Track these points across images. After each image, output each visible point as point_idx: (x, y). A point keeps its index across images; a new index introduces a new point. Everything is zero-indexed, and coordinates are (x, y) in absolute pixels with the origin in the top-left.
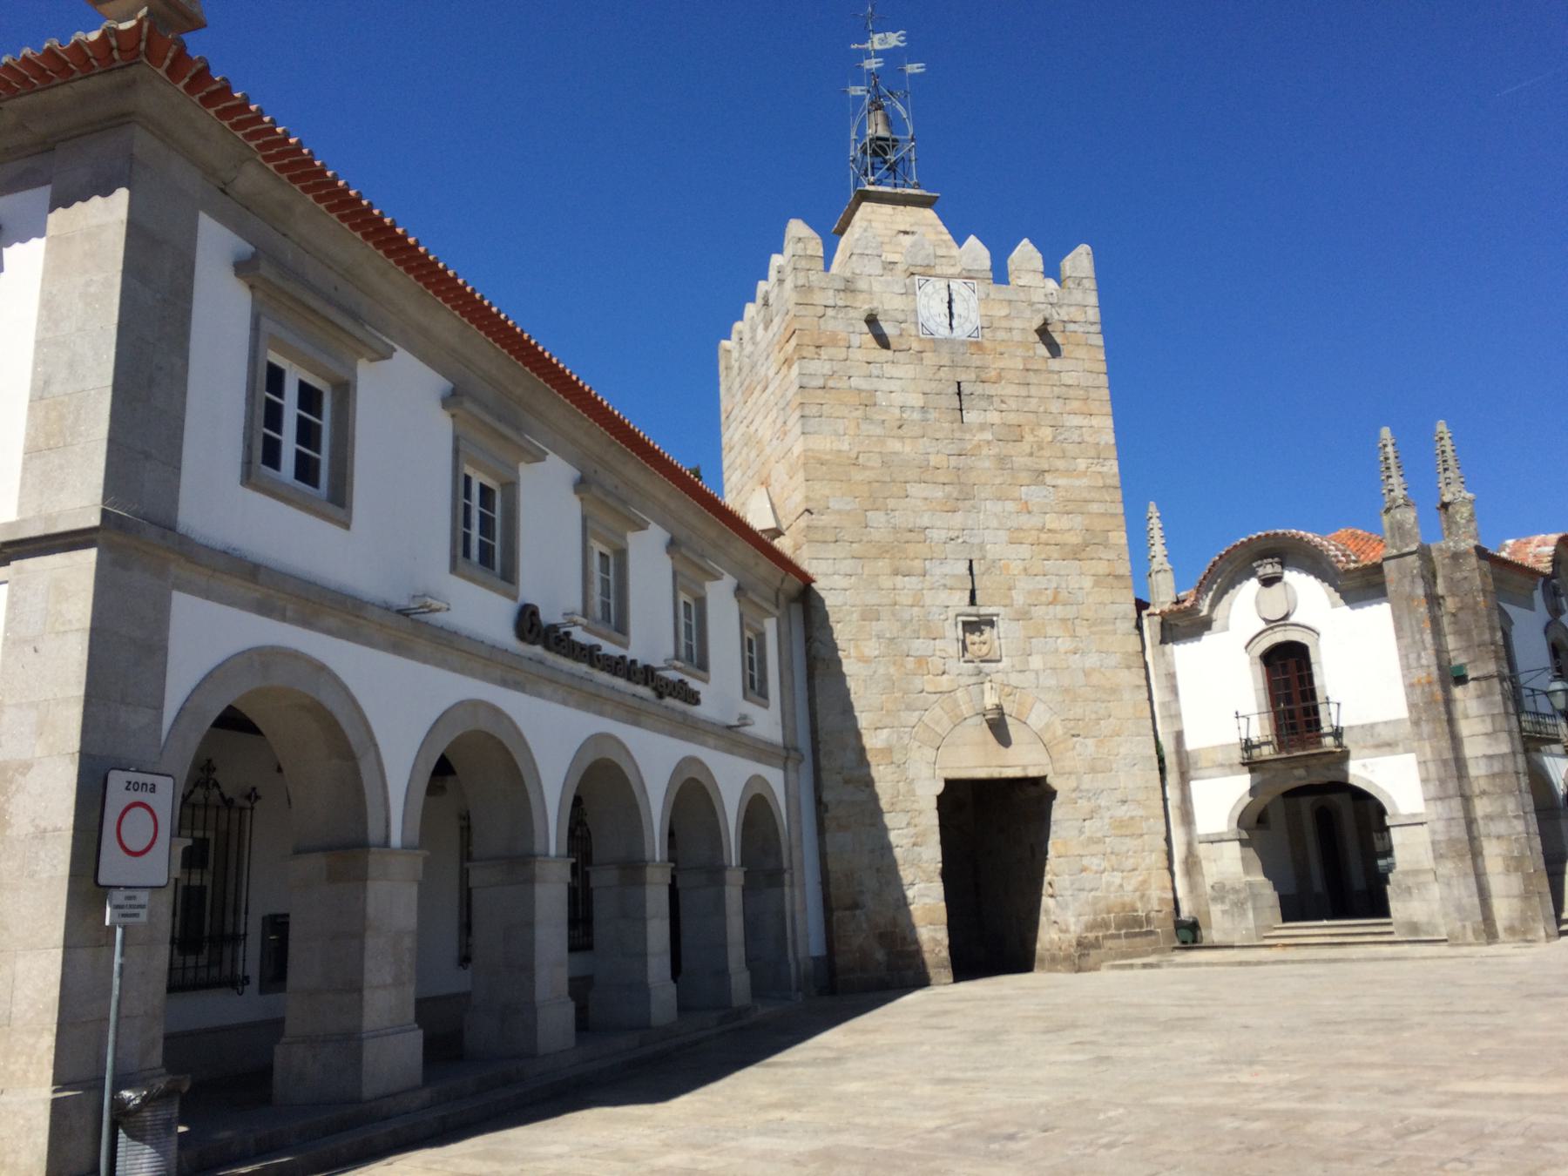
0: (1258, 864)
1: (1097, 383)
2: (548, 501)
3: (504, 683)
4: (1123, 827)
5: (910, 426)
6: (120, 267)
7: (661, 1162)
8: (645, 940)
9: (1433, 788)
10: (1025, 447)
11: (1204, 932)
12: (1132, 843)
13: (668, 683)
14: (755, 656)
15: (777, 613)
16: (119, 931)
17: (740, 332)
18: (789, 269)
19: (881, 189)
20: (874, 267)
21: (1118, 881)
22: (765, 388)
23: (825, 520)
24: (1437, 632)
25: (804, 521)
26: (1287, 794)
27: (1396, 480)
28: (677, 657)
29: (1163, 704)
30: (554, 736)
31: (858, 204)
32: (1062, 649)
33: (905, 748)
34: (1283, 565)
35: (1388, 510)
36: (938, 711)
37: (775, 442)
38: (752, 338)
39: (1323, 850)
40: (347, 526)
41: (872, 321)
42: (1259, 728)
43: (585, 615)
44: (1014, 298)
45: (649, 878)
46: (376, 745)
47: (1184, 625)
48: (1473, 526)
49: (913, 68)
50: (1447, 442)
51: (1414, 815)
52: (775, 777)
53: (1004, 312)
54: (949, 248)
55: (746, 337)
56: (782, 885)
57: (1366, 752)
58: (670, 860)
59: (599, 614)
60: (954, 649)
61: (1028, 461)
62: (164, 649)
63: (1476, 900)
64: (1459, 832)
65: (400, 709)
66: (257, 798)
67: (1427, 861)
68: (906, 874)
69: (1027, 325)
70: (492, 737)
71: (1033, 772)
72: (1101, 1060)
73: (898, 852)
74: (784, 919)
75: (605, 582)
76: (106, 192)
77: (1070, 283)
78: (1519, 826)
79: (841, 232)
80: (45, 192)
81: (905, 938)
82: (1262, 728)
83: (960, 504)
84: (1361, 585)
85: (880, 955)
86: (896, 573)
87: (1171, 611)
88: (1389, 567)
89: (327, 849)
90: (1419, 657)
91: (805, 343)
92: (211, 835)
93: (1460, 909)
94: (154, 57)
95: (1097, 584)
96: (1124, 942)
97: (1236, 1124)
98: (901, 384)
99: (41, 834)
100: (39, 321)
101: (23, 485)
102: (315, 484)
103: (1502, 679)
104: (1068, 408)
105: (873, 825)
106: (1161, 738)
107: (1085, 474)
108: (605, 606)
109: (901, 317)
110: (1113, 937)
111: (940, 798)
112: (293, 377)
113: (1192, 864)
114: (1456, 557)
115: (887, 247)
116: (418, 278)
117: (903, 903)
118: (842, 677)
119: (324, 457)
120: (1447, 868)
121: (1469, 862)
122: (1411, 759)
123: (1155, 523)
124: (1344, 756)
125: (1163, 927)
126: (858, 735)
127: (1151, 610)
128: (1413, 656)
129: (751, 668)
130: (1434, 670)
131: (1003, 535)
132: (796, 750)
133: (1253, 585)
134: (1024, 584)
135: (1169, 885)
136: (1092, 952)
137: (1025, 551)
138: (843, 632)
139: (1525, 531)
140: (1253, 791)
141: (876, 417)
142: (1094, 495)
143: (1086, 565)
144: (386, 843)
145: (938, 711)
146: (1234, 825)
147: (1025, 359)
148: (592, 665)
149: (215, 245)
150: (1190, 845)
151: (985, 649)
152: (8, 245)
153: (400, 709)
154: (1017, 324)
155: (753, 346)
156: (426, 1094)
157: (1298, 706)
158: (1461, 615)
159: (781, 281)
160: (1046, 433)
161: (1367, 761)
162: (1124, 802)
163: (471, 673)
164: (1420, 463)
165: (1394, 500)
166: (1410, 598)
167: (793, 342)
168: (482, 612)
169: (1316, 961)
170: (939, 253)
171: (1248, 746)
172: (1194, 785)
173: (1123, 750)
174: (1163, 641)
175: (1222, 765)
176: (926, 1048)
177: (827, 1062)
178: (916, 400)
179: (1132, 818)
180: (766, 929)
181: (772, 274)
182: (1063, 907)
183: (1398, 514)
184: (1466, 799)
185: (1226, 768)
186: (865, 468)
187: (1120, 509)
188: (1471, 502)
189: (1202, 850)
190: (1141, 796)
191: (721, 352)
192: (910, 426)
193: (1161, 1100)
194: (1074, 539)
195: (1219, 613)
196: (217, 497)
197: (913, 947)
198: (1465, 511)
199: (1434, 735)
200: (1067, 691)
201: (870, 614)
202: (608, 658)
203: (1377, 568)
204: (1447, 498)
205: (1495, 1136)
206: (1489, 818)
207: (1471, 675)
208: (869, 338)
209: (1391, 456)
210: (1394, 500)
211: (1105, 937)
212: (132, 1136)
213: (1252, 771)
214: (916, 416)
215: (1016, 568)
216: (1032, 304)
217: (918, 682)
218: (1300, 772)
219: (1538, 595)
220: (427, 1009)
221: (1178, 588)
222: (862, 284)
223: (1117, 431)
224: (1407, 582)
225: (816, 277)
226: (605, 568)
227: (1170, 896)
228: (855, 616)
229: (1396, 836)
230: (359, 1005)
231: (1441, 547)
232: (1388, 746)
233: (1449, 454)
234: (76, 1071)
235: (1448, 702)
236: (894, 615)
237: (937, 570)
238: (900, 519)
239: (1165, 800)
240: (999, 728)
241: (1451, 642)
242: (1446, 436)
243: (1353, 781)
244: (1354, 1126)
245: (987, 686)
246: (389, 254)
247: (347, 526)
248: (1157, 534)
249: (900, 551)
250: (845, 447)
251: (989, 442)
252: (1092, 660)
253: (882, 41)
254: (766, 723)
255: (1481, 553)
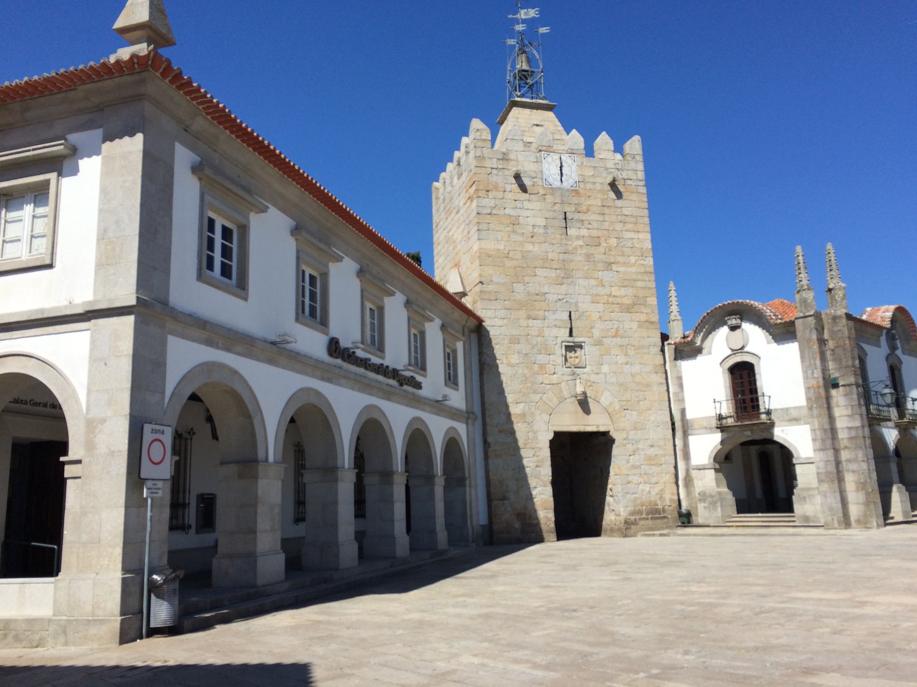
0: (724, 482)
1: (642, 214)
2: (344, 282)
3: (322, 379)
4: (652, 460)
5: (539, 236)
6: (140, 174)
7: (407, 617)
8: (393, 513)
9: (818, 444)
10: (601, 249)
11: (694, 518)
12: (655, 469)
13: (405, 378)
14: (451, 362)
15: (463, 339)
16: (149, 500)
17: (444, 179)
18: (472, 146)
19: (524, 100)
20: (519, 146)
21: (648, 489)
22: (458, 212)
23: (490, 288)
24: (823, 359)
25: (478, 288)
26: (744, 444)
27: (803, 275)
28: (410, 364)
29: (675, 393)
30: (347, 405)
31: (511, 108)
32: (620, 362)
33: (532, 413)
34: (742, 319)
35: (798, 292)
36: (550, 394)
37: (463, 243)
38: (451, 183)
39: (760, 476)
40: (246, 299)
41: (517, 177)
42: (727, 408)
43: (362, 343)
44: (597, 165)
45: (395, 481)
46: (261, 412)
47: (687, 350)
48: (844, 302)
49: (543, 30)
50: (832, 255)
51: (809, 458)
52: (461, 428)
53: (591, 173)
54: (561, 134)
55: (448, 182)
56: (465, 486)
57: (784, 423)
58: (406, 471)
59: (369, 342)
60: (561, 360)
61: (603, 257)
62: (165, 364)
63: (840, 505)
64: (832, 468)
65: (272, 392)
66: (194, 433)
67: (814, 483)
68: (532, 482)
69: (603, 181)
70: (315, 406)
71: (602, 429)
72: (625, 579)
73: (528, 470)
74: (465, 504)
75: (372, 324)
76: (132, 135)
77: (628, 158)
78: (864, 466)
79: (501, 123)
80: (98, 133)
81: (530, 517)
82: (728, 408)
83: (565, 281)
84: (783, 332)
85: (517, 525)
86: (529, 318)
87: (680, 343)
88: (798, 323)
89: (237, 462)
90: (813, 373)
91: (480, 188)
93: (831, 509)
94: (155, 67)
95: (640, 326)
96: (650, 522)
97: (682, 607)
98: (533, 213)
99: (112, 453)
100: (100, 199)
101: (95, 282)
102: (230, 278)
103: (858, 386)
104: (626, 228)
105: (515, 455)
106: (673, 412)
107: (634, 265)
108: (373, 337)
109: (534, 175)
110: (644, 519)
111: (551, 442)
112: (219, 223)
113: (688, 481)
114: (835, 318)
115: (526, 134)
116: (279, 169)
117: (530, 498)
118: (499, 374)
119: (234, 264)
120: (825, 487)
121: (836, 485)
122: (807, 428)
123: (673, 293)
124: (772, 425)
125: (672, 514)
126: (507, 406)
127: (670, 341)
128: (809, 372)
129: (449, 369)
130: (821, 380)
131: (588, 298)
132: (473, 413)
133: (725, 330)
134: (599, 325)
135: (676, 492)
136: (633, 527)
137: (600, 307)
138: (499, 350)
139: (877, 303)
140: (722, 442)
141: (519, 231)
142: (639, 277)
143: (634, 316)
144: (266, 460)
145: (550, 394)
146: (712, 460)
147: (603, 200)
148: (366, 369)
149: (183, 157)
151: (577, 361)
152: (82, 158)
153: (272, 392)
154: (598, 180)
155: (451, 187)
156: (286, 585)
157: (748, 397)
158: (836, 351)
159: (467, 153)
160: (613, 242)
161: (784, 428)
162: (652, 446)
163: (307, 374)
164: (816, 265)
165: (802, 286)
166: (809, 340)
167: (474, 188)
168: (312, 342)
169: (753, 535)
170: (557, 137)
171: (720, 418)
172: (690, 438)
173: (652, 418)
174: (676, 359)
175: (706, 428)
176: (539, 572)
177: (487, 577)
178: (542, 222)
179: (656, 455)
180: (456, 510)
181: (463, 148)
182: (618, 502)
183: (804, 294)
184: (836, 451)
185: (708, 430)
186: (512, 259)
187: (653, 285)
188: (844, 288)
189: (694, 473)
190: (661, 443)
191: (433, 189)
192: (539, 236)
193: (650, 597)
194: (627, 301)
195: (706, 344)
196: (189, 291)
197: (535, 522)
198: (841, 293)
199: (820, 415)
200: (622, 385)
201: (514, 340)
202: (374, 365)
203: (792, 323)
204: (831, 286)
205: (800, 615)
206: (849, 461)
207: (841, 383)
208: (515, 187)
209: (801, 261)
210: (802, 286)
211: (640, 519)
212: (158, 597)
213: (722, 431)
214: (541, 231)
215: (595, 316)
216: (606, 169)
217: (540, 378)
218: (748, 433)
219: (883, 339)
220: (286, 544)
221: (685, 329)
222: (512, 156)
223: (653, 241)
224: (807, 331)
225: (487, 152)
226: (372, 317)
227: (676, 498)
228: (506, 341)
229: (799, 469)
230: (254, 542)
231: (827, 312)
232: (795, 420)
233: (833, 262)
234: (132, 566)
235: (828, 398)
236: (527, 341)
237: (551, 317)
238: (532, 288)
239: (675, 446)
240: (584, 404)
241: (831, 365)
242: (832, 252)
243: (776, 439)
244: (737, 610)
245: (578, 381)
246: (265, 158)
247: (246, 299)
248: (674, 299)
249: (531, 306)
250: (502, 247)
251: (581, 246)
252: (636, 368)
253: (526, 14)
254: (457, 399)
255: (849, 317)
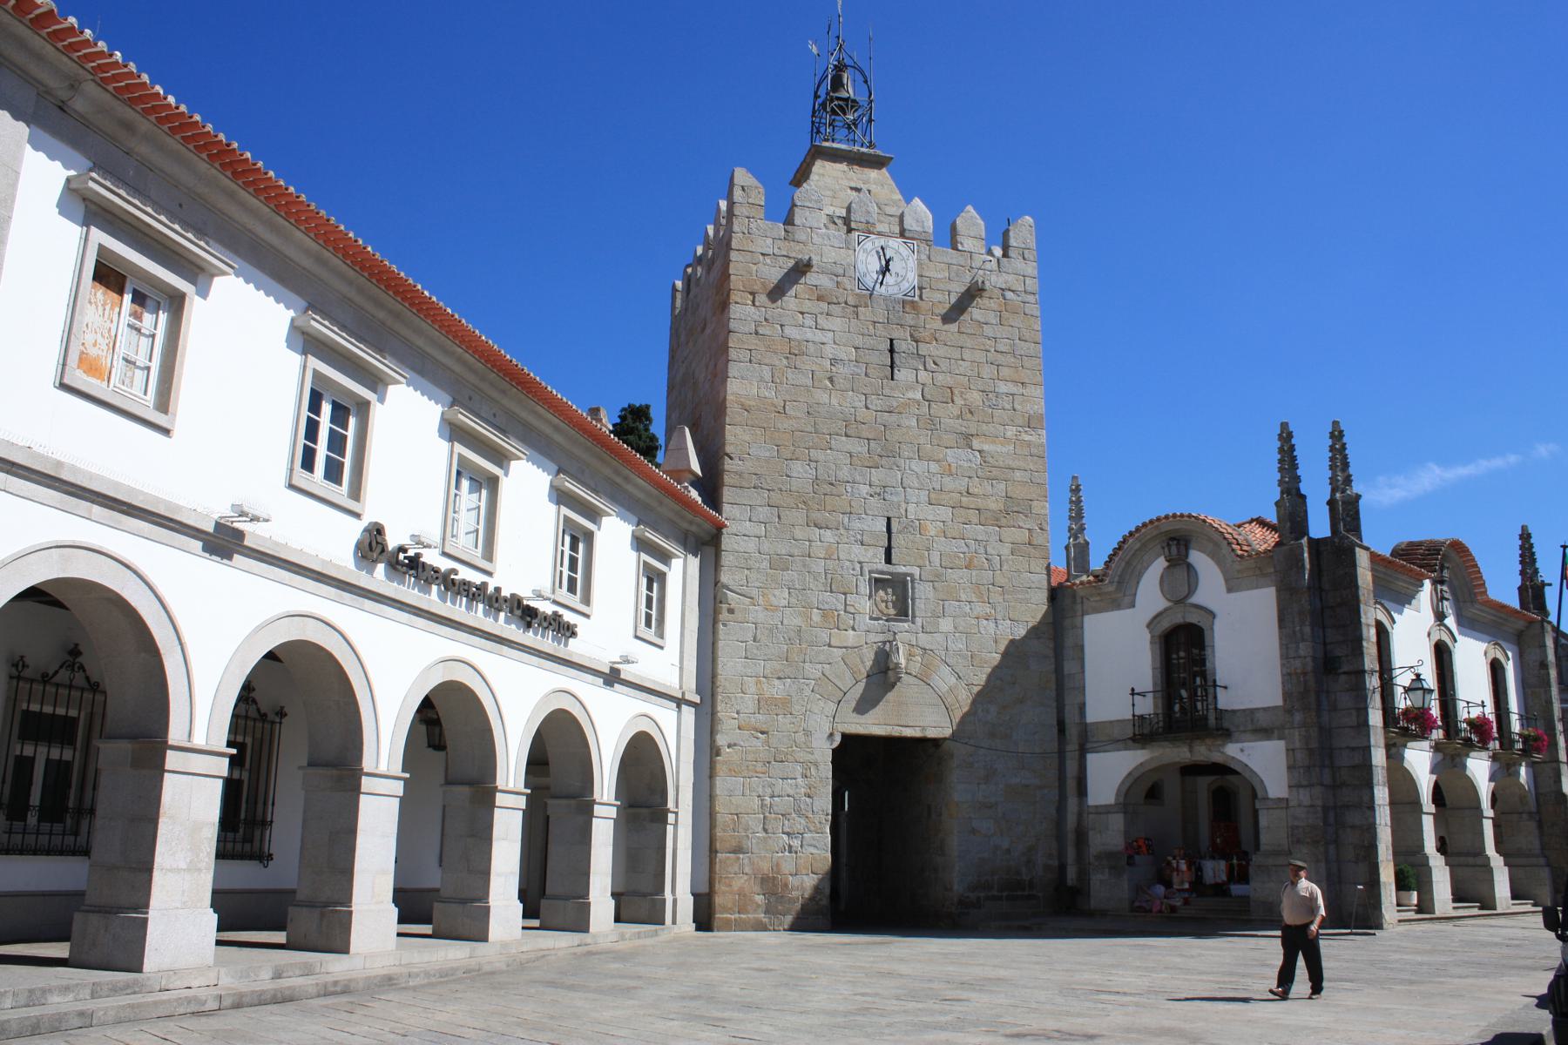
21: (1005, 845)
82: (1156, 706)
83: (884, 461)
92: (249, 740)
102: (338, 481)
113: (1081, 836)
137: (945, 513)
150: (1080, 815)
160: (975, 397)
172: (1090, 757)
232: (1265, 733)
